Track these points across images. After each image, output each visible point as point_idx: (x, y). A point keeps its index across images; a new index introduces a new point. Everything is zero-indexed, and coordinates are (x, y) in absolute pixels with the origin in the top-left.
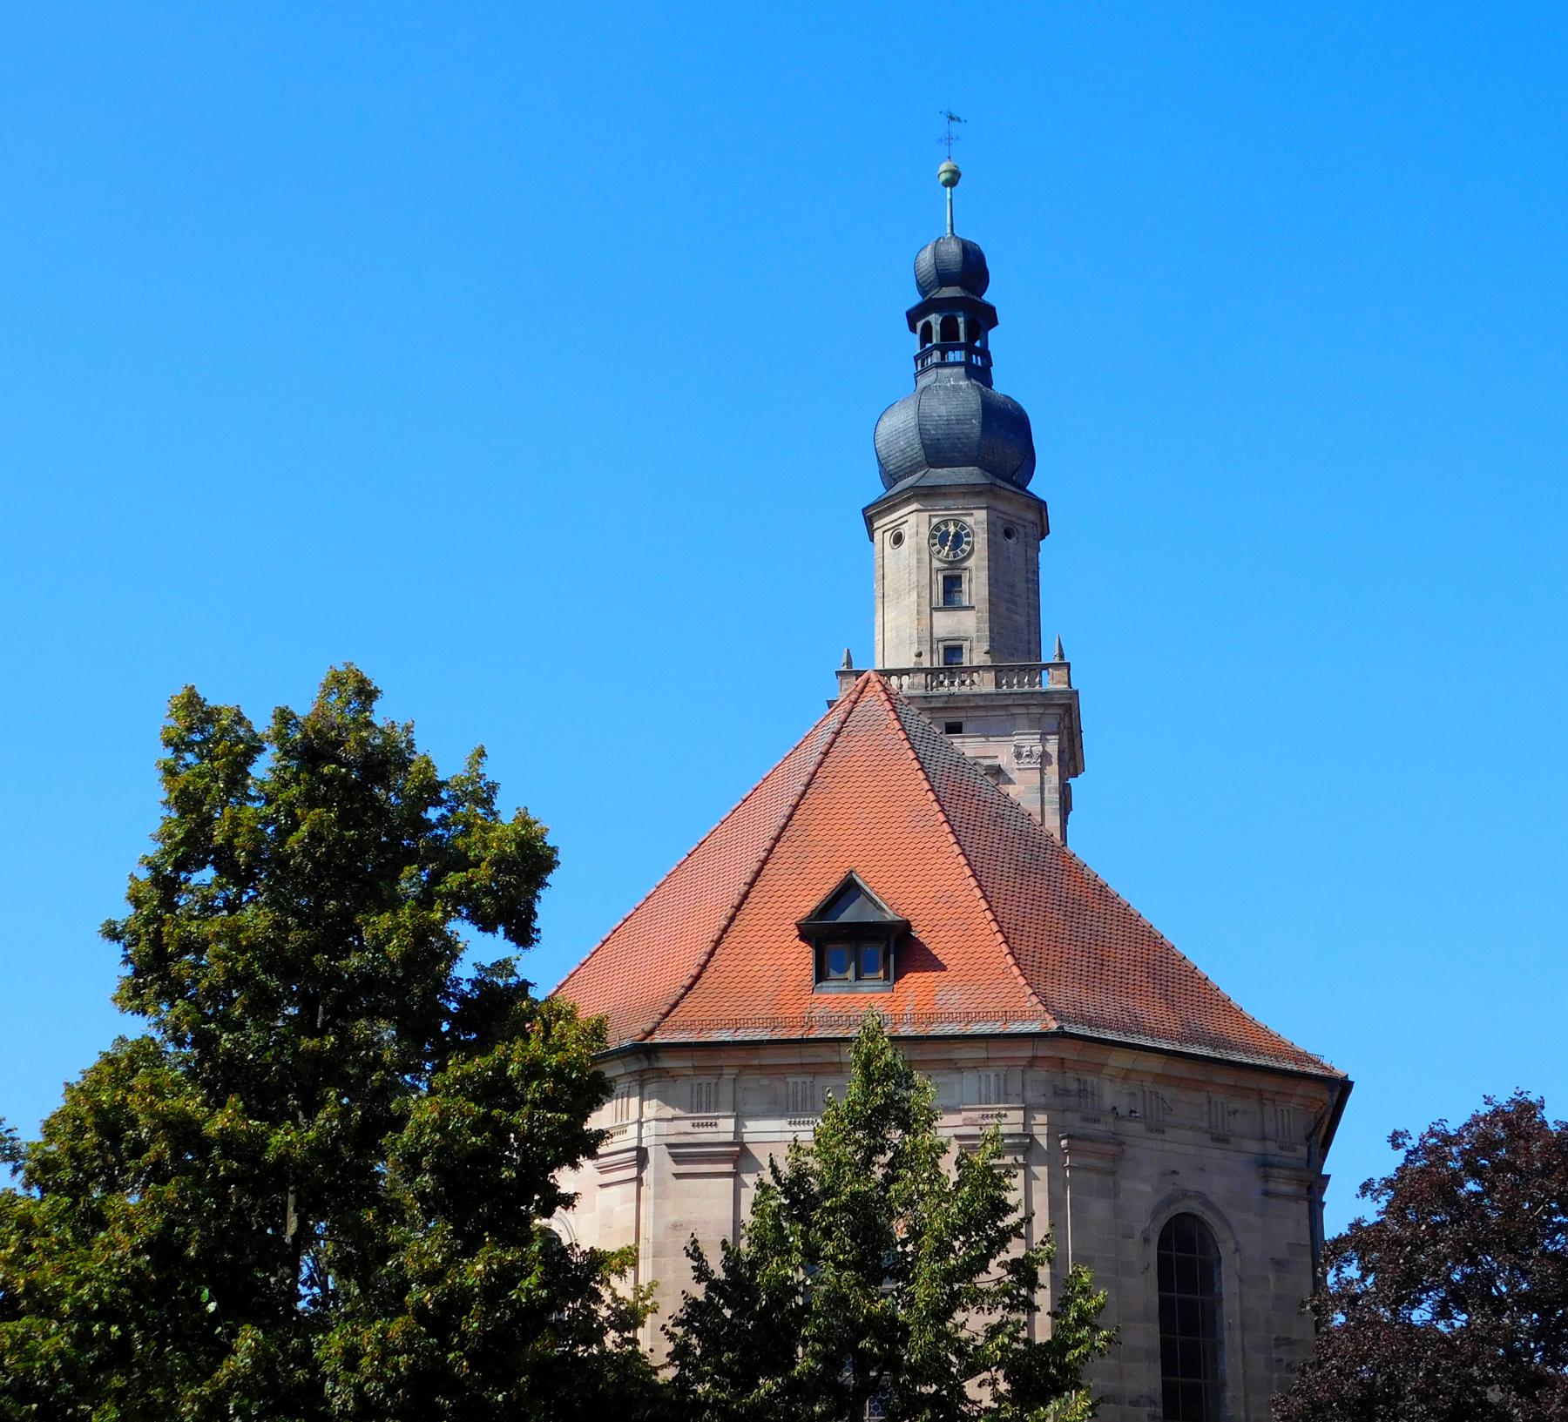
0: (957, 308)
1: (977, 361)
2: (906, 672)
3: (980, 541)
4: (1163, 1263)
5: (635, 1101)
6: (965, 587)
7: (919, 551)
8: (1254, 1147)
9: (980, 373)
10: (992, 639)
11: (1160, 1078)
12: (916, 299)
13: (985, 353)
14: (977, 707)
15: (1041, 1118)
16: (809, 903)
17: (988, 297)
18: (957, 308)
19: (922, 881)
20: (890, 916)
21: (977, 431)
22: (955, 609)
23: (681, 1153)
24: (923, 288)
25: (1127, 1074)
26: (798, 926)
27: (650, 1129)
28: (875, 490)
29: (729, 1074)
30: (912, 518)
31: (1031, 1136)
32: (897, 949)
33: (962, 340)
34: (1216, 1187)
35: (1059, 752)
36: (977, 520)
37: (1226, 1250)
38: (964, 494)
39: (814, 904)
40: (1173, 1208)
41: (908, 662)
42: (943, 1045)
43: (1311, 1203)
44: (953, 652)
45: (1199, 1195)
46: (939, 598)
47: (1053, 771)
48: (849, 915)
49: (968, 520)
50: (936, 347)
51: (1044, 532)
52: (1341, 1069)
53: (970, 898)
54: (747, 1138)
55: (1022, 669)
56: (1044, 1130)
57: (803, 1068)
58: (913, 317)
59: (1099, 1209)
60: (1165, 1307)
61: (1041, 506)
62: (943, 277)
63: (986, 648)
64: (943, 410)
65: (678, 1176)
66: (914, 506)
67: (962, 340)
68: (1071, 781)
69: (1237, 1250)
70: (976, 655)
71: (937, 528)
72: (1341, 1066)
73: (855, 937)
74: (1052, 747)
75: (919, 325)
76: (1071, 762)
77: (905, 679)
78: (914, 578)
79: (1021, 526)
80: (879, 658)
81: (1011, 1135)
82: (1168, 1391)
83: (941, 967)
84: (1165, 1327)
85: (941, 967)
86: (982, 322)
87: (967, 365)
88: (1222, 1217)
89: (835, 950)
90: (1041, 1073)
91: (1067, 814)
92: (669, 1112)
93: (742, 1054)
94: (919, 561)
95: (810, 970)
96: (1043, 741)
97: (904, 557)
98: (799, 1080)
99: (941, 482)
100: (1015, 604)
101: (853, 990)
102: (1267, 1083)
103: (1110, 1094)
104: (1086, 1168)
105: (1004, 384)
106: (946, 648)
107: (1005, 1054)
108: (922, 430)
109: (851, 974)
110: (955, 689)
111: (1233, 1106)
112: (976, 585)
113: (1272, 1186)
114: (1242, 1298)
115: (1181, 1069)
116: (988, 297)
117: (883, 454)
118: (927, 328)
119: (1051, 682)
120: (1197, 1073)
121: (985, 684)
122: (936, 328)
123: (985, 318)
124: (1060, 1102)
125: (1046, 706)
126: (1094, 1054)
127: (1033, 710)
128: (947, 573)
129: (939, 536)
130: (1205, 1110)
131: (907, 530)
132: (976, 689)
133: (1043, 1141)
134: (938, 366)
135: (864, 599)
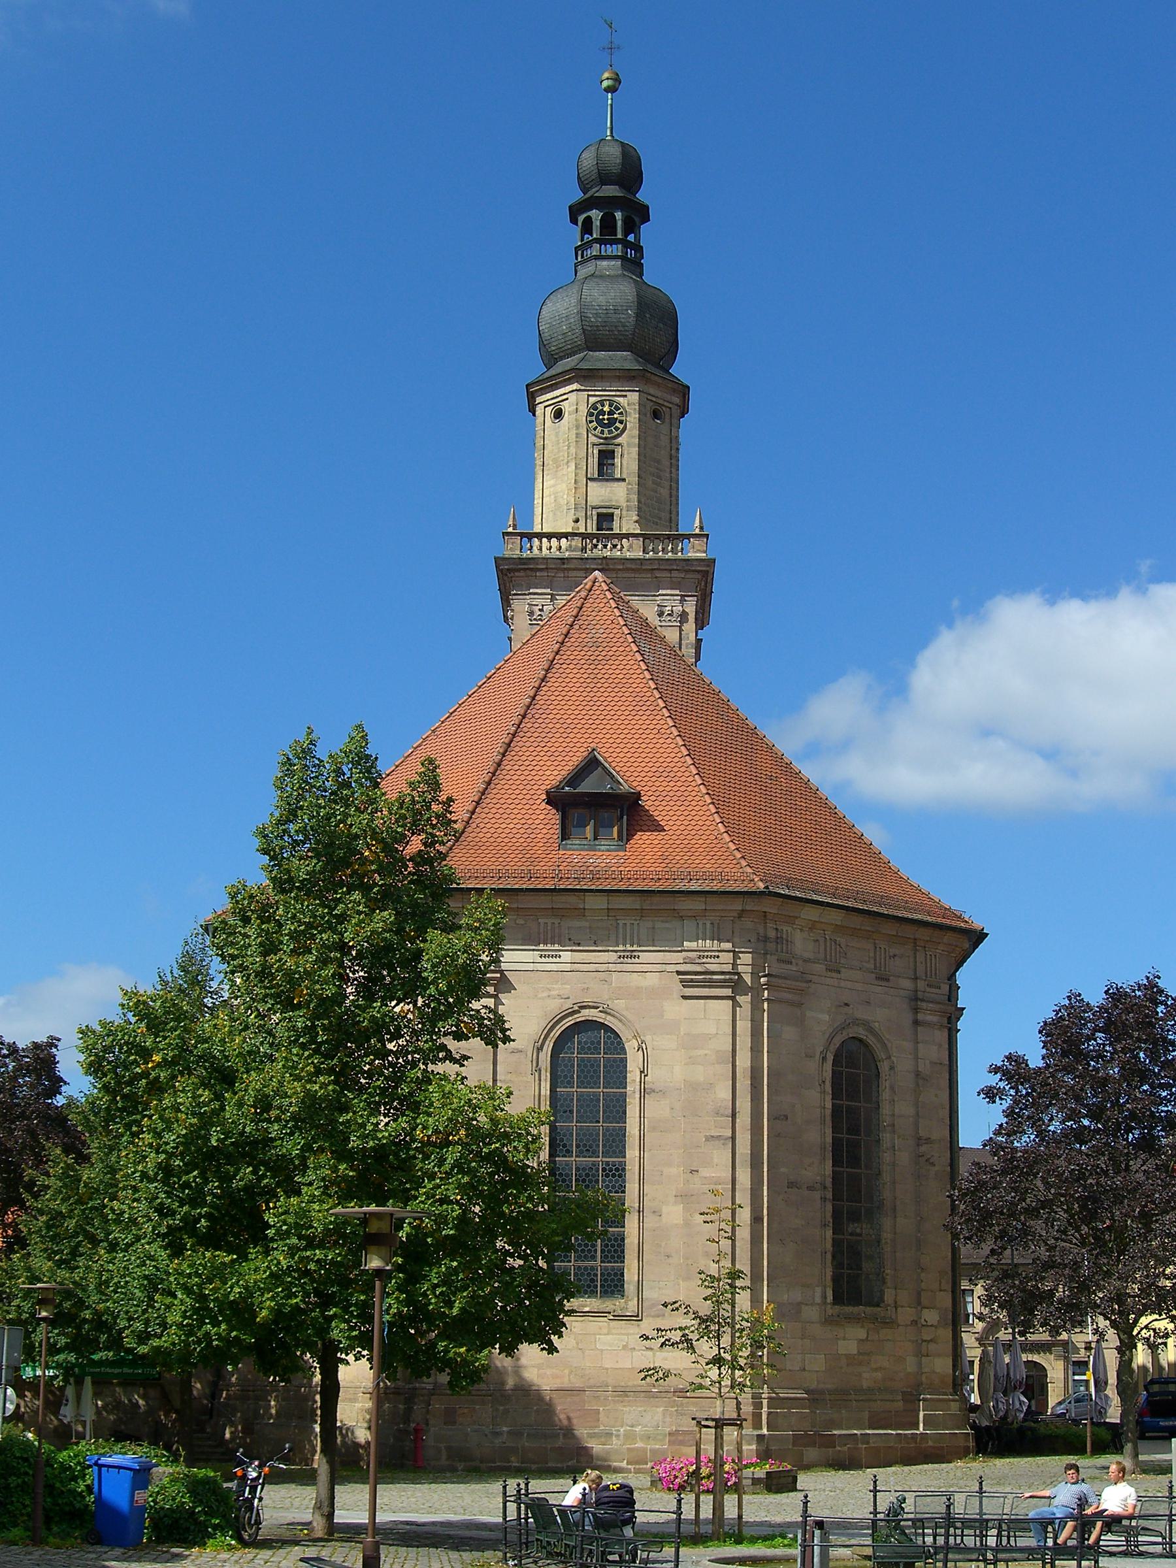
0: (613, 205)
1: (631, 253)
2: (566, 535)
3: (632, 420)
4: (836, 1075)
6: (617, 461)
7: (577, 427)
8: (907, 984)
9: (633, 263)
11: (839, 929)
12: (577, 195)
13: (638, 249)
14: (628, 570)
15: (746, 958)
16: (554, 774)
17: (642, 196)
18: (613, 205)
19: (648, 756)
20: (625, 788)
21: (632, 320)
22: (607, 480)
24: (584, 186)
25: (813, 926)
26: (548, 793)
30: (573, 397)
31: (738, 974)
33: (619, 236)
34: (879, 1016)
36: (630, 401)
37: (884, 1067)
38: (619, 378)
40: (845, 1033)
43: (950, 1029)
44: (605, 519)
45: (867, 1025)
46: (594, 471)
47: (690, 626)
49: (621, 400)
50: (596, 241)
51: (684, 411)
53: (687, 774)
54: (504, 966)
55: (669, 537)
56: (749, 969)
57: (554, 912)
58: (574, 212)
59: (789, 1033)
60: (836, 1112)
62: (604, 178)
63: (636, 518)
64: (602, 300)
66: (575, 386)
69: (892, 1068)
70: (627, 523)
71: (594, 407)
73: (595, 804)
74: (691, 607)
75: (581, 218)
77: (564, 540)
78: (573, 450)
79: (668, 405)
80: (537, 519)
81: (723, 973)
82: (836, 1177)
83: (659, 828)
84: (835, 1129)
85: (659, 828)
86: (637, 219)
87: (623, 258)
89: (575, 814)
95: (557, 830)
96: (682, 600)
97: (562, 432)
98: (549, 921)
99: (599, 365)
100: (659, 477)
101: (592, 848)
102: (923, 934)
103: (801, 944)
104: (780, 1001)
106: (599, 515)
107: (720, 907)
108: (582, 316)
109: (589, 830)
111: (892, 951)
112: (627, 461)
113: (920, 1017)
114: (896, 1107)
115: (856, 921)
116: (642, 196)
117: (546, 336)
118: (588, 222)
119: (694, 551)
121: (633, 550)
122: (597, 223)
123: (638, 214)
124: (768, 946)
125: (687, 571)
127: (675, 574)
128: (601, 447)
129: (595, 413)
130: (872, 955)
131: (565, 406)
133: (748, 979)
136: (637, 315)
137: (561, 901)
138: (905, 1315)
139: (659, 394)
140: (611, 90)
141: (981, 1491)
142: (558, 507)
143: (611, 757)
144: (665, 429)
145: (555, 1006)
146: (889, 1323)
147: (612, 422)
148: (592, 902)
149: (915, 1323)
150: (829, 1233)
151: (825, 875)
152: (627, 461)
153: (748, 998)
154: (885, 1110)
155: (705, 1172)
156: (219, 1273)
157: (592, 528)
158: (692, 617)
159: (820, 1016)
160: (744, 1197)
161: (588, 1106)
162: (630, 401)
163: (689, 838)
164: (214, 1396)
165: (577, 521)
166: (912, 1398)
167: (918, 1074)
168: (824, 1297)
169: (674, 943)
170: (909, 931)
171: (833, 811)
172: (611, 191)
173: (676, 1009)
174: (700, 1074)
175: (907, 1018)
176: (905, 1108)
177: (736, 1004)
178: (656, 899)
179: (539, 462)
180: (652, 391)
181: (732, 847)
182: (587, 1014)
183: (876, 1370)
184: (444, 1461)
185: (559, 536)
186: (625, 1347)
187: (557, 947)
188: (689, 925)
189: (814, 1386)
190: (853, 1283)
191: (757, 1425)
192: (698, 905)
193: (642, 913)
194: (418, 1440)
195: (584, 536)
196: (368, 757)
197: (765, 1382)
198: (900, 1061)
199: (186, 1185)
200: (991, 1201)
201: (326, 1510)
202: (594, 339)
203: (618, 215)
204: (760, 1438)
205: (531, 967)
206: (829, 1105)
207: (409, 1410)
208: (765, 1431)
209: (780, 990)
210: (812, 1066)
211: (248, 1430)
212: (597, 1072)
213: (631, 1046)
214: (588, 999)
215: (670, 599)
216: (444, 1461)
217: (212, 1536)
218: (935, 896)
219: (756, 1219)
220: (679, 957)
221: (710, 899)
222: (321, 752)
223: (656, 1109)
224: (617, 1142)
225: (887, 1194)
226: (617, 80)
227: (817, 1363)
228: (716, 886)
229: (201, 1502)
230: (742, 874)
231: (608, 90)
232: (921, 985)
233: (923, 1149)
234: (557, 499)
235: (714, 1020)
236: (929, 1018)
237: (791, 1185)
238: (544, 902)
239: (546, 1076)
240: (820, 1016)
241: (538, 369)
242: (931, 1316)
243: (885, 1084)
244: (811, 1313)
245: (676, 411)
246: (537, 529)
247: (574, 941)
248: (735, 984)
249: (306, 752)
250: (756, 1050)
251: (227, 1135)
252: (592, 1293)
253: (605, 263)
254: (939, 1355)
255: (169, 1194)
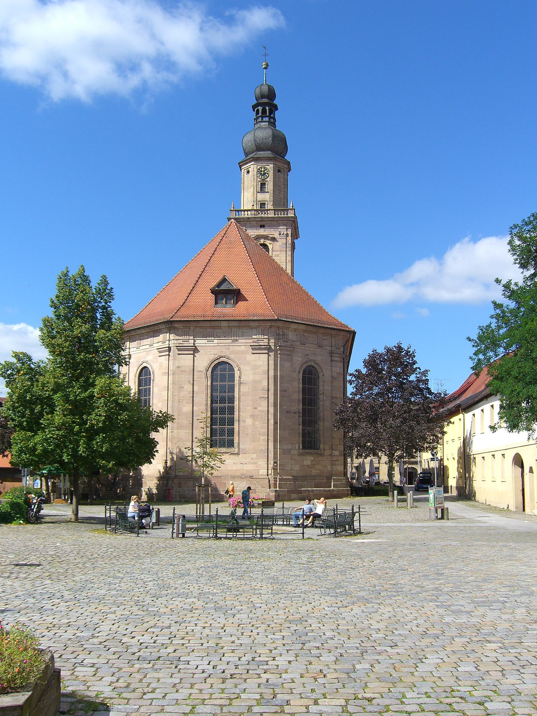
0: (266, 105)
2: (250, 210)
3: (271, 173)
5: (168, 334)
6: (266, 186)
9: (272, 123)
10: (273, 201)
11: (304, 331)
13: (274, 118)
15: (272, 341)
16: (213, 283)
17: (275, 102)
18: (266, 105)
19: (243, 278)
20: (235, 287)
21: (271, 141)
23: (180, 348)
25: (295, 330)
27: (172, 342)
28: (243, 157)
29: (192, 328)
30: (252, 166)
31: (270, 346)
32: (236, 295)
33: (268, 114)
35: (292, 234)
36: (270, 167)
37: (321, 375)
38: (267, 160)
39: (215, 283)
41: (250, 208)
42: (247, 322)
44: (263, 205)
45: (314, 361)
47: (289, 238)
48: (223, 287)
50: (260, 116)
52: (353, 329)
55: (282, 210)
57: (212, 327)
58: (254, 107)
59: (287, 364)
61: (288, 163)
62: (263, 97)
65: (178, 354)
66: (253, 163)
67: (268, 114)
68: (296, 241)
70: (269, 206)
72: (352, 327)
73: (226, 293)
74: (289, 232)
75: (256, 110)
76: (295, 235)
77: (249, 212)
78: (252, 183)
79: (283, 169)
80: (242, 206)
82: (304, 409)
83: (247, 300)
85: (247, 300)
87: (269, 122)
88: (319, 366)
89: (220, 296)
90: (273, 329)
91: (294, 250)
92: (177, 338)
93: (196, 323)
94: (254, 178)
102: (333, 332)
103: (291, 336)
105: (279, 126)
109: (224, 301)
110: (263, 216)
112: (270, 186)
113: (333, 358)
114: (325, 387)
115: (310, 328)
116: (275, 102)
117: (244, 147)
118: (258, 110)
119: (291, 214)
120: (314, 329)
121: (271, 215)
122: (260, 111)
124: (278, 337)
126: (287, 325)
127: (284, 221)
129: (259, 171)
131: (250, 170)
132: (269, 216)
133: (273, 347)
134: (260, 122)
135: (237, 190)
136: (272, 140)
137: (213, 324)
138: (327, 452)
139: (280, 164)
140: (266, 68)
141: (283, 507)
142: (248, 202)
143: (229, 278)
144: (282, 175)
145: (212, 357)
146: (322, 455)
147: (265, 174)
148: (223, 324)
149: (331, 455)
150: (301, 427)
151: (302, 313)
152: (270, 186)
153: (273, 353)
154: (321, 388)
155: (259, 408)
156: (28, 439)
157: (259, 208)
158: (290, 235)
159: (298, 359)
160: (271, 417)
161: (223, 388)
162: (270, 167)
163: (256, 302)
164: (115, 479)
165: (253, 205)
166: (329, 478)
167: (332, 377)
168: (299, 447)
169: (250, 336)
170: (329, 331)
171: (307, 294)
172: (265, 100)
173: (250, 357)
174: (257, 378)
175: (330, 359)
176: (327, 388)
177: (269, 355)
178: (243, 322)
179: (242, 188)
180: (277, 164)
181: (269, 305)
182: (222, 359)
183: (317, 470)
184: (178, 499)
185: (248, 211)
186: (234, 463)
187: (213, 338)
188: (254, 331)
189: (295, 475)
190: (310, 442)
191: (276, 487)
192: (256, 324)
193: (239, 327)
194: (169, 492)
195: (255, 210)
196: (85, 276)
197: (278, 474)
198: (327, 372)
199: (19, 412)
200: (349, 416)
201: (75, 513)
202: (259, 148)
203: (267, 108)
204: (276, 491)
205: (204, 345)
206: (301, 387)
207: (167, 483)
208: (278, 489)
209: (283, 350)
210: (295, 375)
211: (124, 490)
212: (226, 377)
213: (236, 369)
214: (222, 355)
215: (283, 229)
216: (178, 499)
217: (15, 520)
218: (339, 320)
219: (275, 423)
220: (251, 341)
221: (260, 322)
222: (70, 275)
223: (243, 389)
224: (231, 400)
225: (321, 414)
226: (267, 65)
227: (297, 468)
228: (262, 318)
229: (13, 510)
230: (270, 314)
231: (264, 68)
232: (333, 348)
233: (334, 400)
234: (248, 199)
235: (262, 361)
236: (336, 359)
237: (287, 412)
238: (208, 324)
239: (209, 379)
240: (298, 359)
241: (243, 157)
242: (336, 453)
243: (321, 380)
244: (295, 452)
245: (286, 170)
246: (242, 209)
247: (218, 336)
248: (269, 349)
249: (66, 275)
250: (275, 370)
251: (33, 396)
252: (224, 447)
253: (263, 123)
254: (339, 465)
255: (15, 415)
